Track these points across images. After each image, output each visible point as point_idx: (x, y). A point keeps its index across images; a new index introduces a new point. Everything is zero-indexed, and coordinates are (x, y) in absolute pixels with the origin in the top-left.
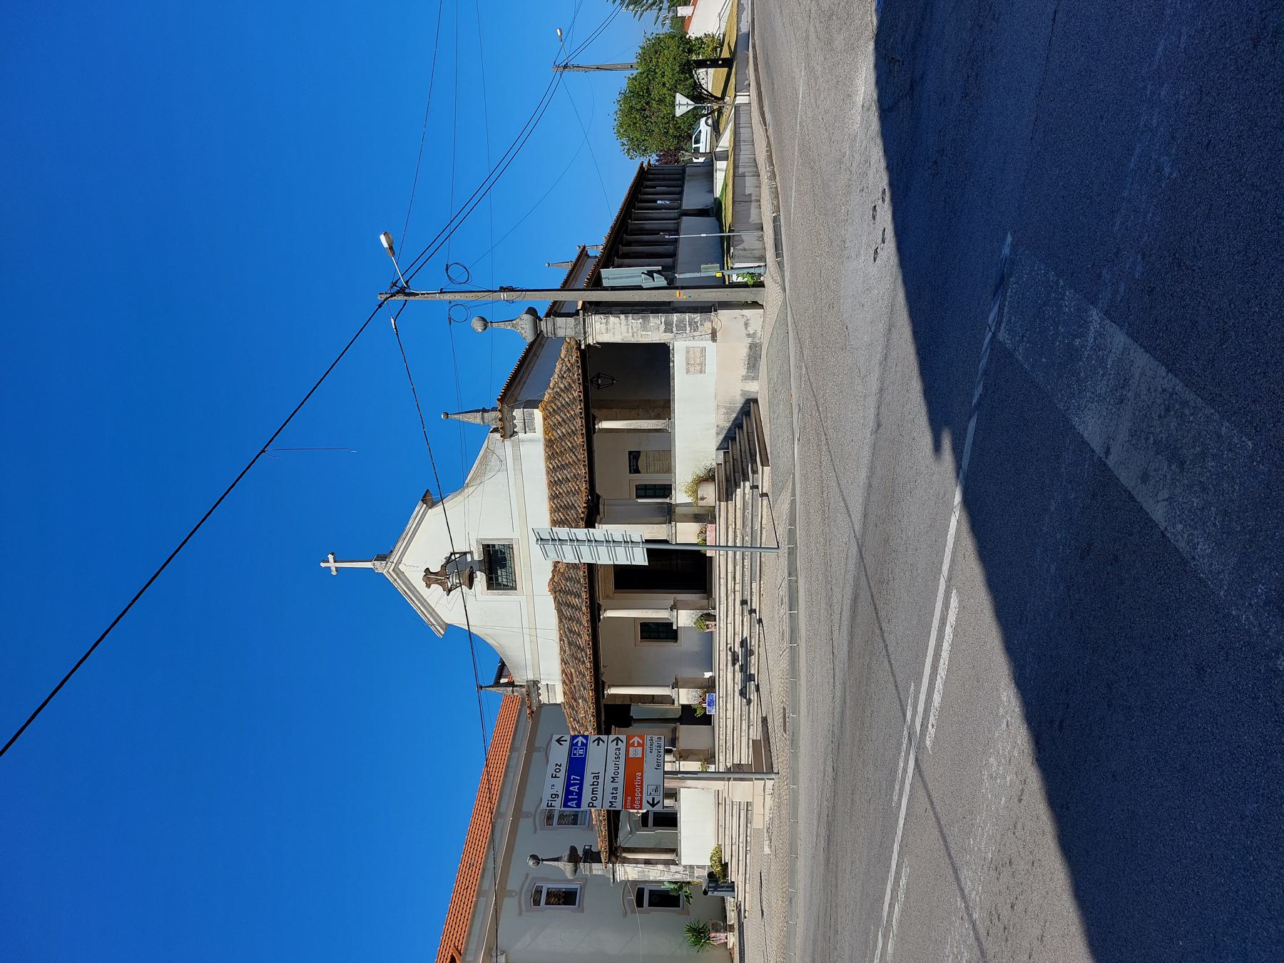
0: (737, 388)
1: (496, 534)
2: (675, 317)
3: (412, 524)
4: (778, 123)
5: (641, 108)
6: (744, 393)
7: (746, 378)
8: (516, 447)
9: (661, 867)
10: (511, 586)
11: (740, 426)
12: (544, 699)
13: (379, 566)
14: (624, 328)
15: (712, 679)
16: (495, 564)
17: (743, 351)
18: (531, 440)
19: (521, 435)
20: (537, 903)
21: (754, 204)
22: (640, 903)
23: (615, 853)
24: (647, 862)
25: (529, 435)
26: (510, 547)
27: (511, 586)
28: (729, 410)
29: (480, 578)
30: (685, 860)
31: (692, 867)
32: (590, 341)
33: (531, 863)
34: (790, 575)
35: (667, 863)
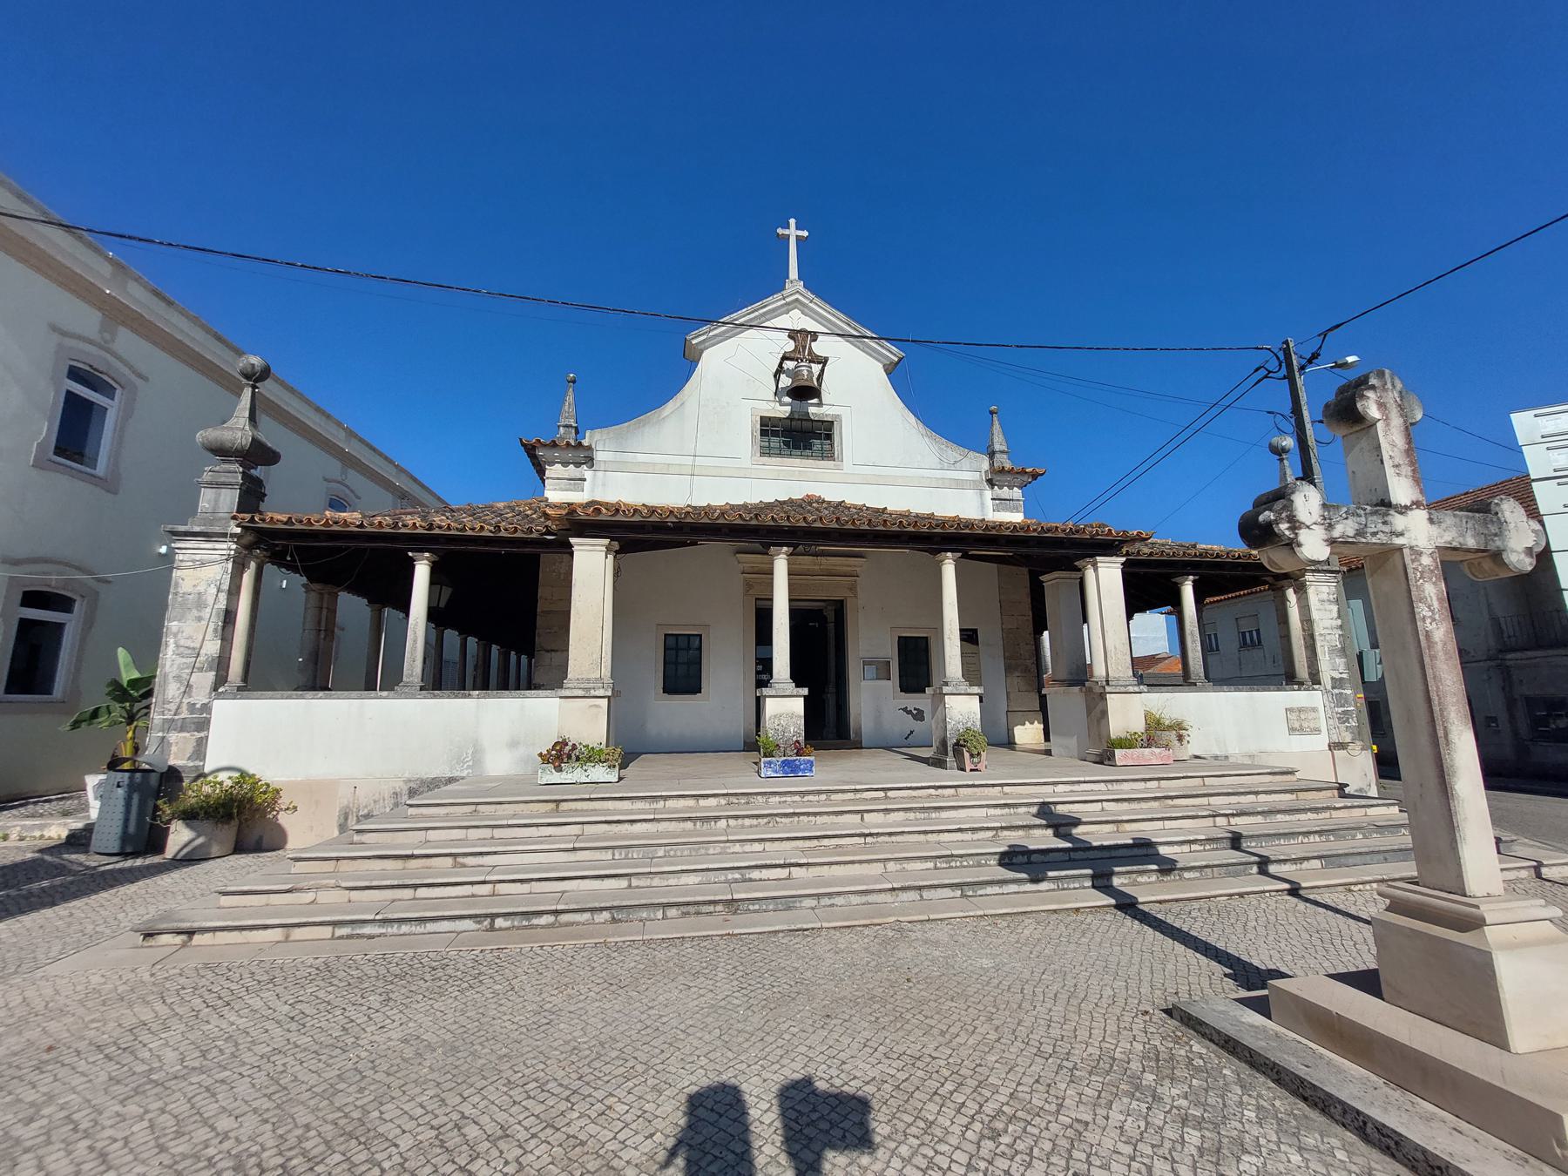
1: (848, 438)
8: (974, 485)
9: (212, 647)
10: (766, 452)
14: (1328, 623)
15: (1010, 744)
16: (799, 431)
19: (988, 494)
20: (74, 374)
22: (32, 598)
23: (268, 545)
24: (229, 617)
25: (989, 503)
26: (832, 457)
29: (782, 410)
30: (226, 712)
31: (203, 725)
33: (256, 360)
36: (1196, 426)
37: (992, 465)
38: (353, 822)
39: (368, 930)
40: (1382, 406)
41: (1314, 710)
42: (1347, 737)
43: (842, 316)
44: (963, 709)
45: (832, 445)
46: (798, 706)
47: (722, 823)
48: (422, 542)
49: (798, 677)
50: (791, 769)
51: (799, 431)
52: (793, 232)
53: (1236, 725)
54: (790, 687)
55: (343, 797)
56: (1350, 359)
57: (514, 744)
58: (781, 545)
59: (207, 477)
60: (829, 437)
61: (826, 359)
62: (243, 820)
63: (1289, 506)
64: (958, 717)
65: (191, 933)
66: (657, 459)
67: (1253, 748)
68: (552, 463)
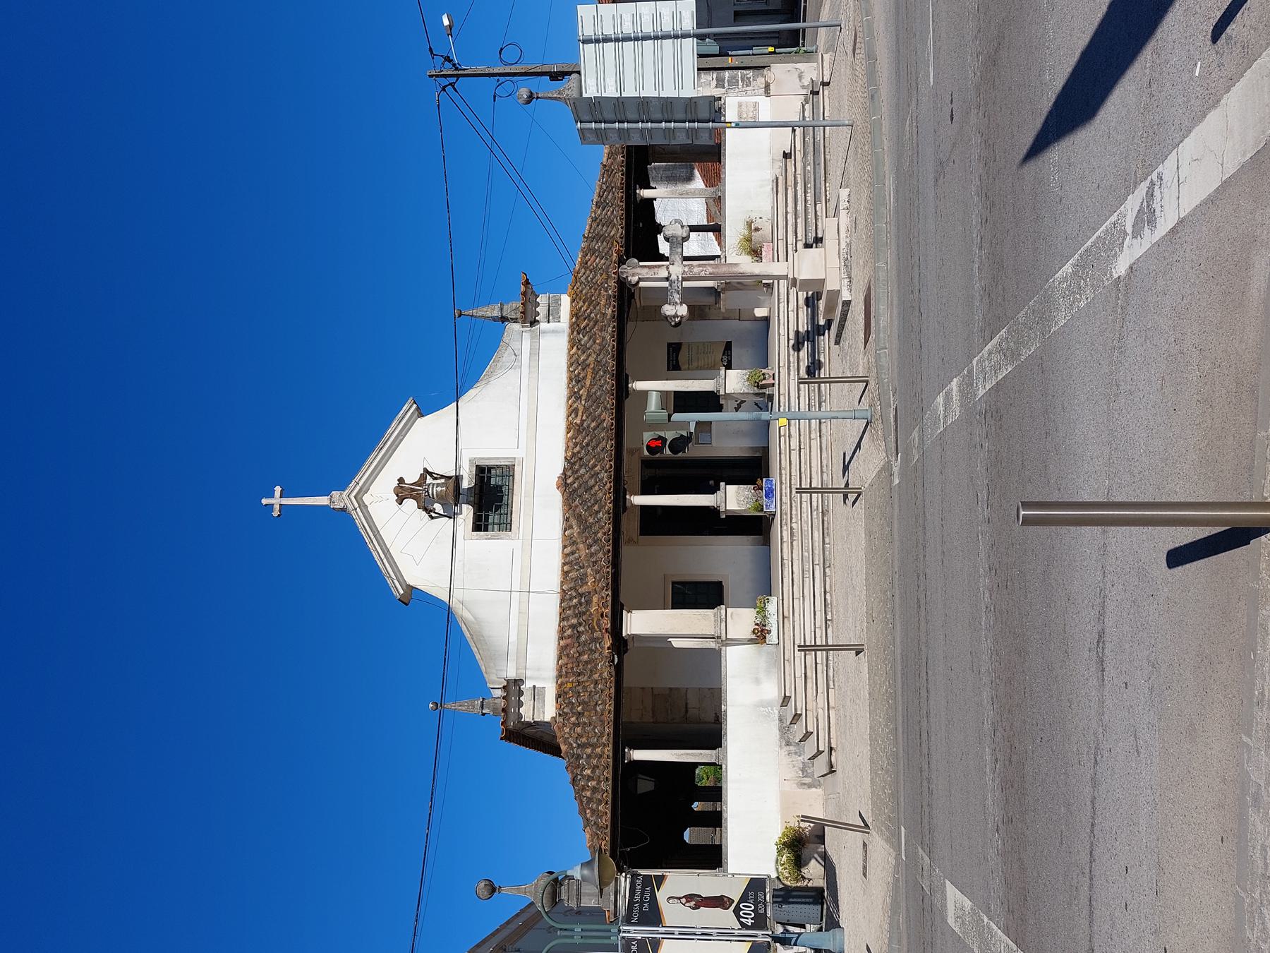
1: (492, 451)
3: (395, 428)
8: (536, 338)
10: (506, 525)
12: (527, 714)
15: (766, 320)
16: (487, 497)
18: (554, 332)
19: (543, 326)
25: (552, 325)
26: (511, 468)
27: (506, 525)
29: (467, 512)
36: (517, 179)
37: (515, 320)
38: (807, 780)
39: (831, 674)
40: (633, 275)
41: (740, 106)
42: (761, 81)
43: (373, 455)
44: (734, 381)
45: (498, 466)
46: (732, 489)
47: (794, 525)
48: (618, 754)
49: (713, 490)
50: (770, 493)
51: (487, 497)
52: (276, 500)
53: (750, 163)
54: (720, 494)
55: (791, 787)
56: (446, 22)
57: (757, 681)
58: (625, 498)
59: (573, 904)
60: (490, 468)
61: (426, 471)
62: (801, 845)
63: (670, 317)
64: (740, 385)
65: (831, 749)
66: (514, 623)
67: (767, 159)
68: (520, 716)
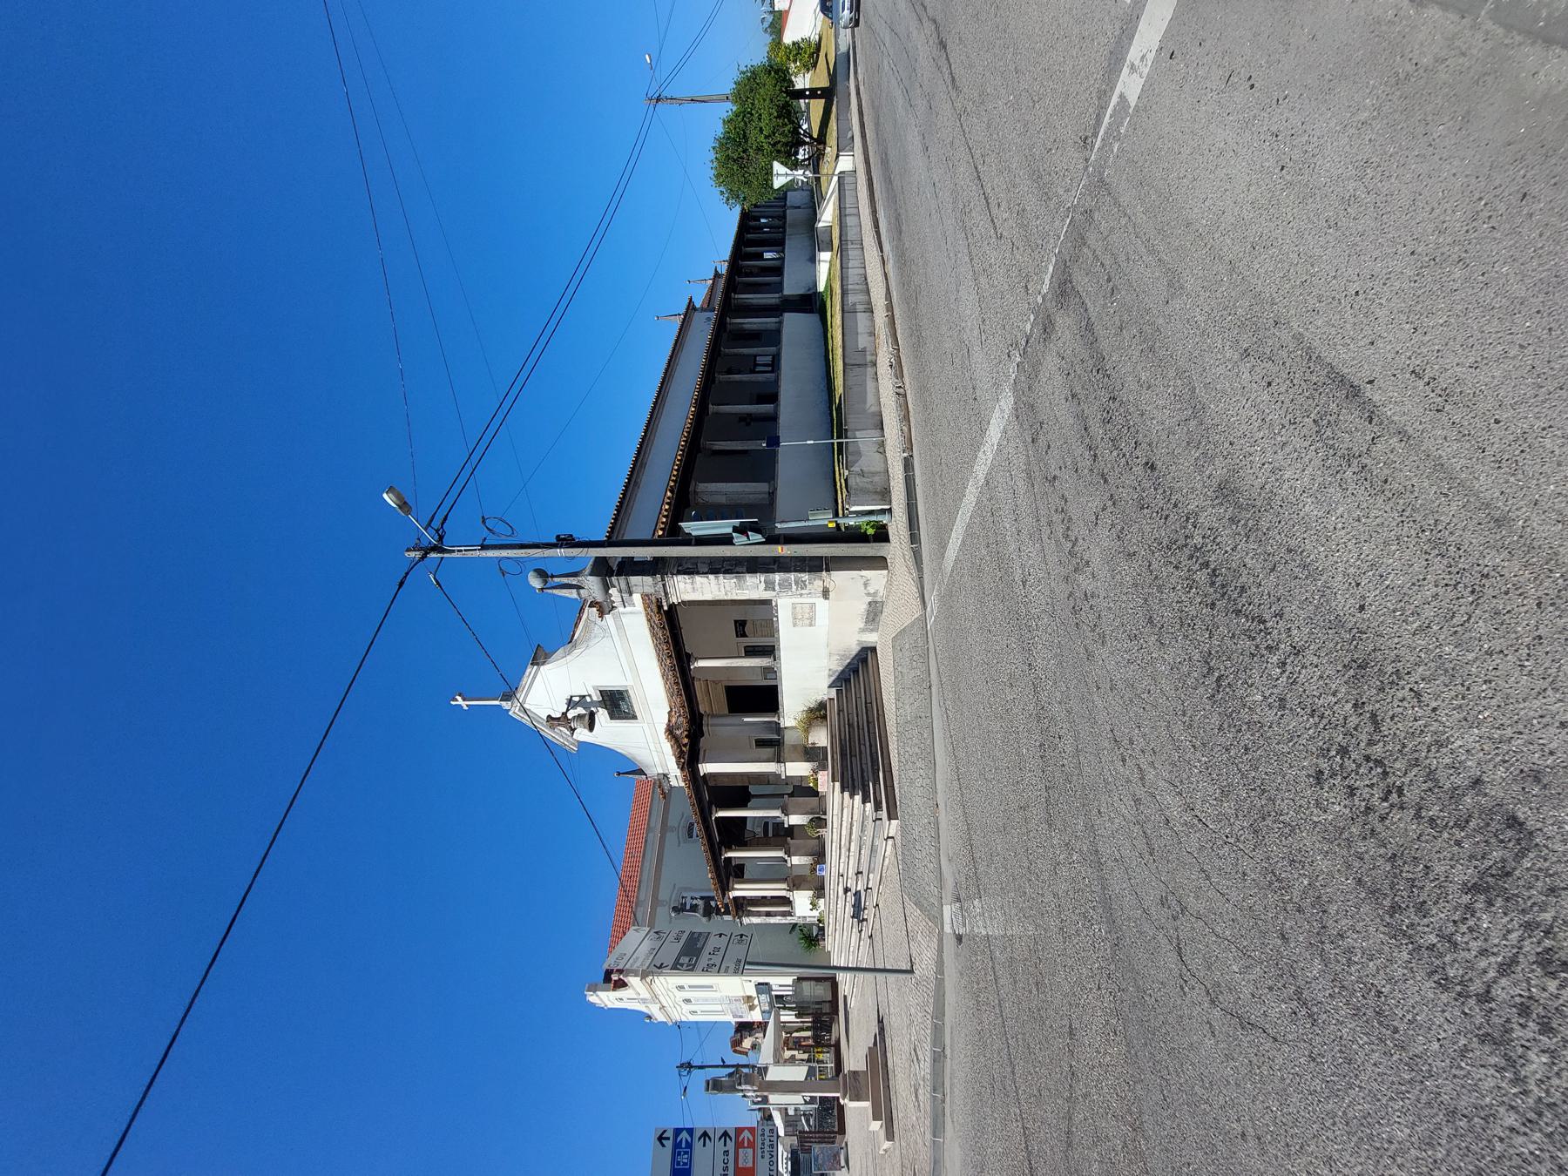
0: (853, 639)
1: (613, 682)
2: (777, 577)
4: (918, 342)
5: (738, 158)
6: (860, 642)
7: (863, 631)
8: (618, 618)
11: (856, 671)
13: (506, 705)
17: (862, 607)
21: (870, 370)
25: (628, 609)
28: (843, 657)
32: (674, 600)
34: (935, 1090)
35: (784, 914)
